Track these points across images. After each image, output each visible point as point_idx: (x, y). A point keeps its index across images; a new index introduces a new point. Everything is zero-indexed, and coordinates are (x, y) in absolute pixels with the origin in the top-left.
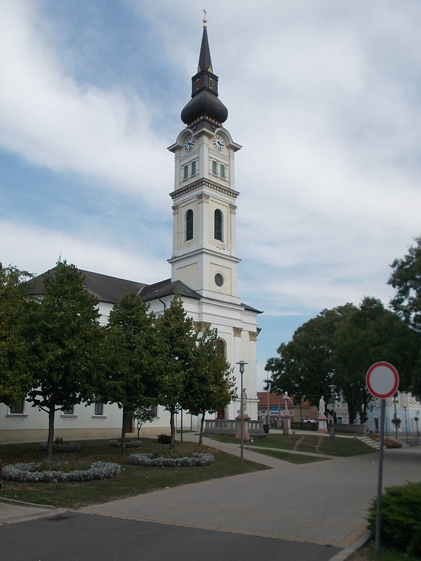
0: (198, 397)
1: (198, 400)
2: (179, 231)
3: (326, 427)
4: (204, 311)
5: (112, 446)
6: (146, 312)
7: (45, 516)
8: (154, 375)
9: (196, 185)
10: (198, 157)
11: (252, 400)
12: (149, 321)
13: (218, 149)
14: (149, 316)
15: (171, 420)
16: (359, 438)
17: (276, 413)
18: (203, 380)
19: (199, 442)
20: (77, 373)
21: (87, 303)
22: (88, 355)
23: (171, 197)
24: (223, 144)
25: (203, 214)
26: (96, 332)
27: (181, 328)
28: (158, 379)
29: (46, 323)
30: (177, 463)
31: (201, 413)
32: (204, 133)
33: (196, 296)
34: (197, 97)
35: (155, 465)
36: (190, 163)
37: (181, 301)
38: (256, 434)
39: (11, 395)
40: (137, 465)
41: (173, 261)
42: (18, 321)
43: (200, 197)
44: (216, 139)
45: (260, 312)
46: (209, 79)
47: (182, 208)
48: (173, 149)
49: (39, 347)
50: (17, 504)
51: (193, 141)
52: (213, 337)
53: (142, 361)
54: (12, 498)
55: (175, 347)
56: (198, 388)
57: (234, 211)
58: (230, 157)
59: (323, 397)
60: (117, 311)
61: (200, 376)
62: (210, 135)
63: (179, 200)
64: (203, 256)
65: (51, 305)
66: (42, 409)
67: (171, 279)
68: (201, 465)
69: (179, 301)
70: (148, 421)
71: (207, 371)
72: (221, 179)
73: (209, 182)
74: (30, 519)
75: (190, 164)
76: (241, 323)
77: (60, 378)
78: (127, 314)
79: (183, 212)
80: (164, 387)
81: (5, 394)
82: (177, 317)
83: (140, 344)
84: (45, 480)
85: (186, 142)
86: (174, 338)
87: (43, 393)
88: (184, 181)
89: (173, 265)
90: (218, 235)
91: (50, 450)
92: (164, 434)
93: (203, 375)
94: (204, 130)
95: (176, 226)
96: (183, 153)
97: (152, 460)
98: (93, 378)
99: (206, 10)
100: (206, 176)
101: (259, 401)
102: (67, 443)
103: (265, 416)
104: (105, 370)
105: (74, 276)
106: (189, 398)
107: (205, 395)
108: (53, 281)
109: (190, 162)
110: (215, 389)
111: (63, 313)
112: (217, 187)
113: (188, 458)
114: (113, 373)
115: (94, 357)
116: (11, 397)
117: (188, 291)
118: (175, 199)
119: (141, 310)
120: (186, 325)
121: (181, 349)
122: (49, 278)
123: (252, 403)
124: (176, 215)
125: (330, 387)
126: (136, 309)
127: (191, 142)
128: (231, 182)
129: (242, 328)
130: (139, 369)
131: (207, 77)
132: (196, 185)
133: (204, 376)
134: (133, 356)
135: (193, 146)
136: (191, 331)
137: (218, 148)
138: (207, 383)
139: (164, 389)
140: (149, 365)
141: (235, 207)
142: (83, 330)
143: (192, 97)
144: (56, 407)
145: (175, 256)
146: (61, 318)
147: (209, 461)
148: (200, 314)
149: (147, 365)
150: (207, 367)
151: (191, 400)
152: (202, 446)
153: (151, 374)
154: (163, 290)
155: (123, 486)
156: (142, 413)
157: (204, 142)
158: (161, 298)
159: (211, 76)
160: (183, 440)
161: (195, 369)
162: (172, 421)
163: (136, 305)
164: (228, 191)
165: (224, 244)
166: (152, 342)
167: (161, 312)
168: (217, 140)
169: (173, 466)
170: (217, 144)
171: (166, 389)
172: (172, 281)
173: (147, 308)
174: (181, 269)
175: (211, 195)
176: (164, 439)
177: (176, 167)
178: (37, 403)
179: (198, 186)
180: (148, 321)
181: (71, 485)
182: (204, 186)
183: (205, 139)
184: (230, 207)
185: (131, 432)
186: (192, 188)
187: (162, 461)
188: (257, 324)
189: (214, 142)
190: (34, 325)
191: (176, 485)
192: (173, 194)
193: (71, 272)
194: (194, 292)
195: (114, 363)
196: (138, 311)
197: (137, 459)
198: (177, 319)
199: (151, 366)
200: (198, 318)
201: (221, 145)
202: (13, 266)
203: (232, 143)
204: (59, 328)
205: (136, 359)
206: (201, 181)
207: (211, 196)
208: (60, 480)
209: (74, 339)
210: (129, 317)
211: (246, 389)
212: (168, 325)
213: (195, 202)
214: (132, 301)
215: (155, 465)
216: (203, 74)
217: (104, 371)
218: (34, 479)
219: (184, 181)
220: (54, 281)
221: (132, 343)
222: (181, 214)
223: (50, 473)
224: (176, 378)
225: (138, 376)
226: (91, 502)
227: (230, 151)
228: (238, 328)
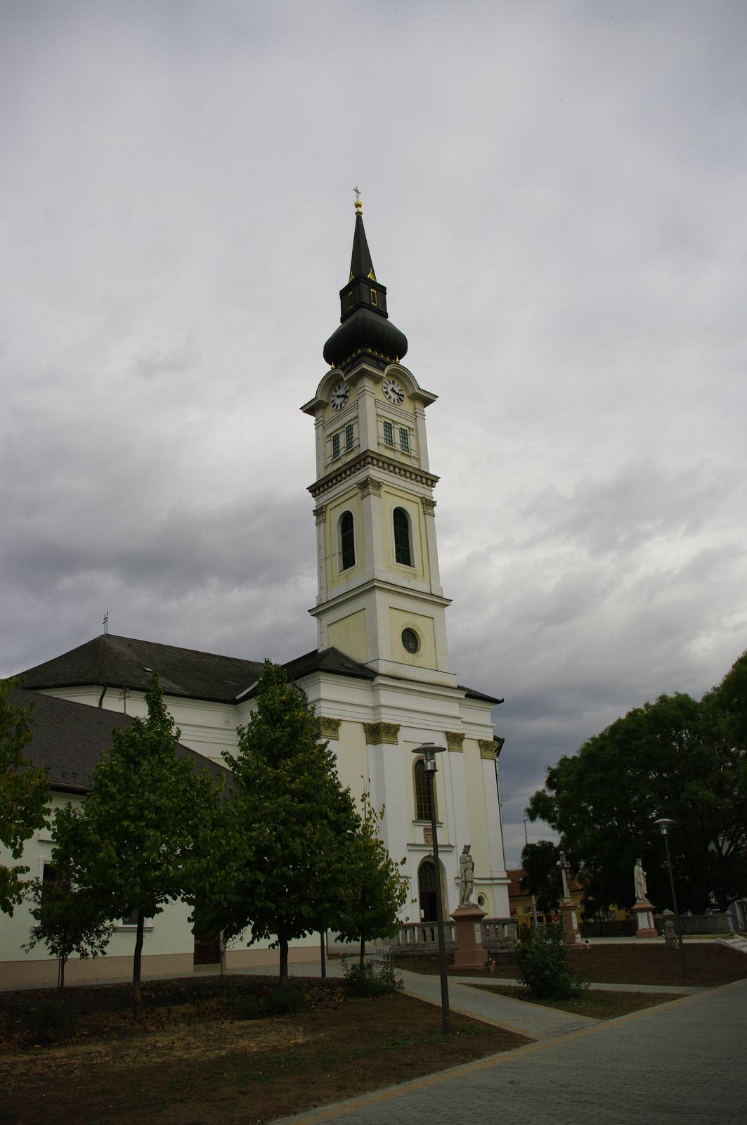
2: (328, 555)
3: (653, 926)
4: (383, 701)
9: (355, 466)
10: (357, 417)
11: (495, 882)
16: (729, 942)
25: (371, 515)
32: (364, 373)
33: (363, 674)
34: (348, 321)
36: (342, 430)
43: (364, 485)
51: (346, 390)
58: (417, 414)
63: (325, 498)
64: (375, 595)
73: (379, 458)
75: (344, 431)
76: (460, 723)
79: (334, 516)
85: (334, 393)
88: (333, 463)
90: (404, 555)
94: (365, 366)
95: (323, 546)
96: (329, 413)
101: (509, 881)
109: (342, 427)
112: (394, 467)
118: (319, 497)
123: (494, 887)
124: (322, 525)
125: (658, 824)
128: (421, 458)
129: (464, 734)
131: (366, 286)
132: (355, 466)
141: (433, 504)
143: (341, 322)
148: (376, 708)
157: (366, 388)
164: (416, 475)
165: (415, 572)
168: (390, 387)
170: (391, 393)
174: (335, 625)
177: (318, 439)
179: (358, 466)
182: (370, 466)
183: (367, 384)
186: (348, 473)
188: (493, 725)
189: (385, 390)
192: (314, 487)
194: (362, 666)
200: (372, 717)
203: (417, 391)
206: (364, 457)
213: (356, 497)
219: (333, 463)
228: (455, 734)
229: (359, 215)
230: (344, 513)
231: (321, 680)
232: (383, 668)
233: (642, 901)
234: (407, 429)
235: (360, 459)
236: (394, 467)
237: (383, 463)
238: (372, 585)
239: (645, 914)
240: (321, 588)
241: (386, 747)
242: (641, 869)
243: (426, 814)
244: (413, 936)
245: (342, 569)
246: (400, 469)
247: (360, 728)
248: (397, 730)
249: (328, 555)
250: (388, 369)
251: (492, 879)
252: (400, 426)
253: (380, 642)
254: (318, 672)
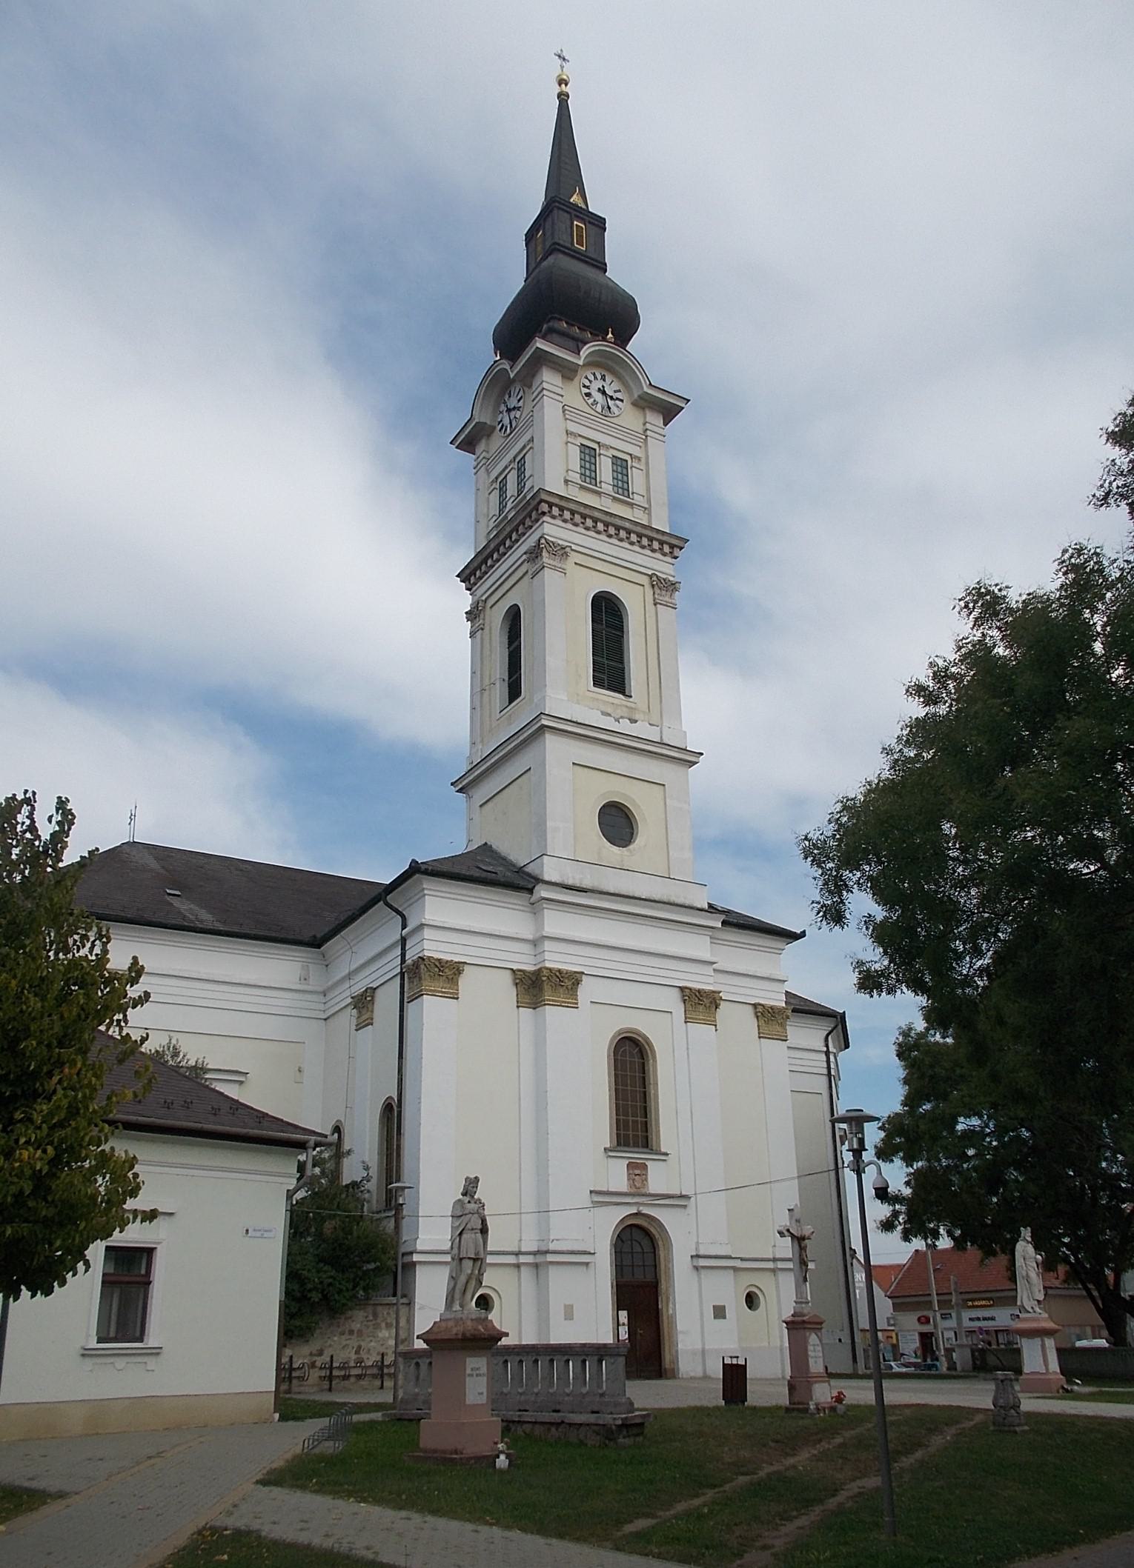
3: (1054, 1366)
4: (549, 929)
10: (532, 440)
13: (599, 409)
17: (985, 1319)
23: (464, 584)
24: (618, 395)
32: (541, 359)
38: (592, 1418)
43: (535, 554)
44: (590, 381)
45: (793, 937)
46: (573, 223)
48: (469, 441)
57: (667, 599)
58: (648, 433)
59: (1026, 1233)
62: (564, 367)
72: (614, 498)
73: (563, 503)
79: (496, 617)
94: (538, 345)
95: (478, 673)
99: (565, 54)
100: (554, 485)
103: (950, 1329)
112: (595, 521)
124: (478, 634)
127: (513, 402)
135: (518, 414)
137: (599, 406)
157: (545, 385)
159: (577, 216)
160: (871, 1384)
165: (633, 705)
170: (598, 397)
175: (574, 547)
179: (528, 522)
182: (546, 518)
183: (549, 379)
184: (653, 586)
194: (520, 871)
200: (531, 960)
201: (611, 398)
203: (646, 389)
207: (572, 550)
211: (477, 1179)
213: (526, 578)
216: (551, 211)
222: (491, 628)
227: (645, 418)
229: (563, 98)
231: (426, 892)
232: (550, 871)
233: (1028, 1315)
234: (628, 458)
235: (529, 509)
236: (595, 521)
237: (573, 512)
238: (539, 725)
239: (1038, 1341)
241: (552, 1014)
242: (1030, 1249)
243: (636, 1136)
246: (607, 525)
247: (508, 977)
248: (577, 983)
249: (487, 682)
250: (585, 351)
251: (775, 1260)
252: (580, 441)
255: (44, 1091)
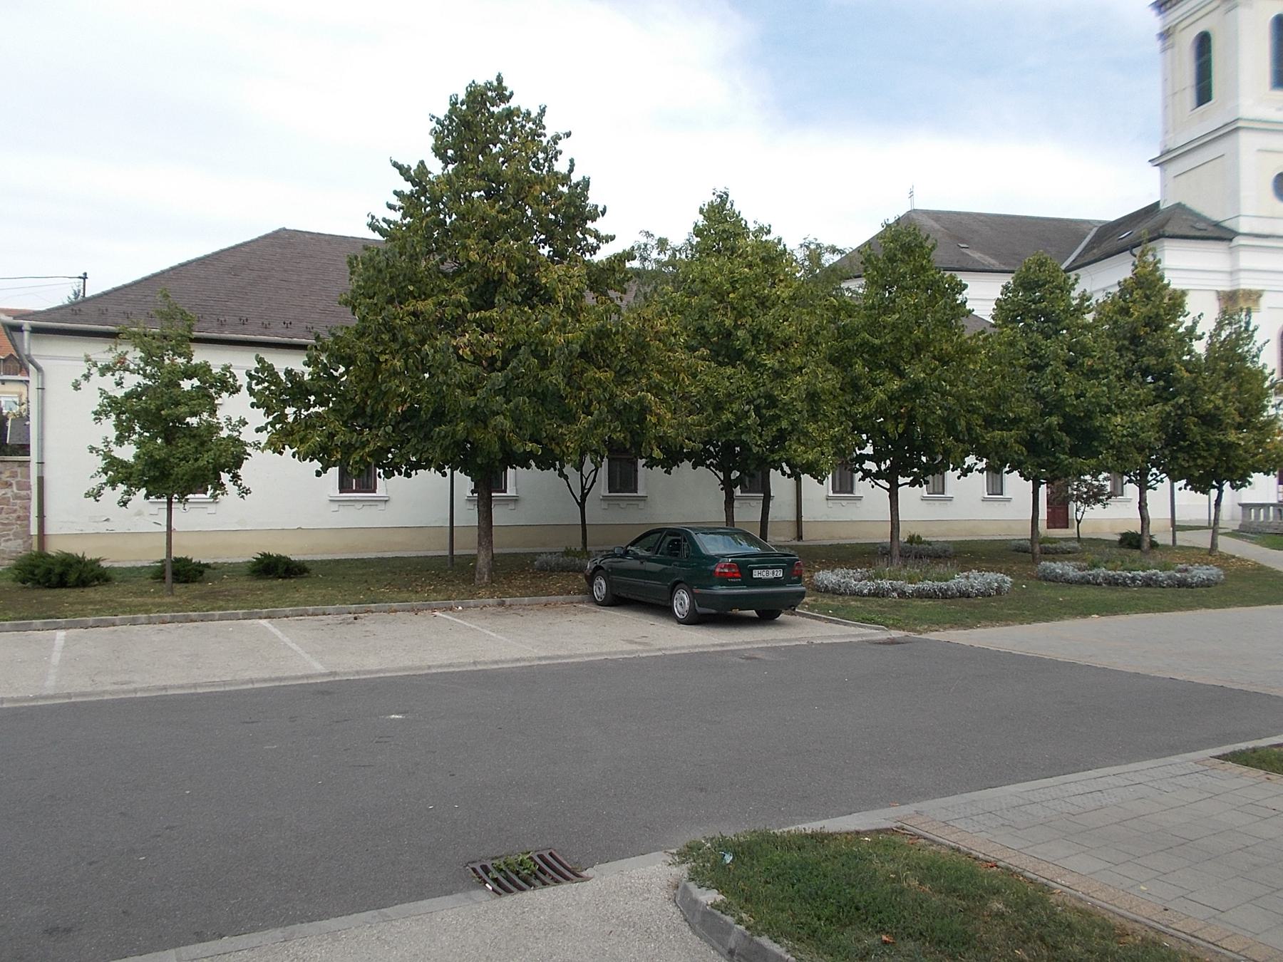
0: (1200, 456)
1: (1199, 462)
5: (1019, 551)
6: (1072, 292)
7: (870, 638)
8: (1089, 415)
12: (1080, 310)
14: (1078, 300)
15: (1139, 503)
18: (1211, 420)
19: (1209, 547)
20: (929, 420)
21: (943, 292)
22: (948, 387)
26: (961, 344)
27: (1157, 315)
28: (1098, 424)
29: (870, 338)
30: (1133, 579)
31: (1214, 487)
33: (1220, 234)
35: (1088, 582)
37: (1158, 258)
39: (817, 461)
40: (1053, 581)
41: (1164, 160)
42: (820, 339)
47: (1183, 32)
49: (861, 379)
50: (831, 621)
52: (1241, 327)
53: (1061, 390)
54: (826, 614)
55: (1143, 356)
56: (1198, 438)
60: (1009, 297)
61: (1203, 413)
65: (876, 303)
66: (876, 484)
67: (1159, 202)
68: (1190, 586)
69: (1151, 259)
70: (1099, 506)
71: (1220, 403)
74: (848, 640)
77: (900, 431)
78: (1029, 301)
79: (1186, 40)
80: (1112, 439)
81: (807, 461)
82: (1146, 294)
83: (1057, 356)
84: (878, 594)
86: (1140, 337)
87: (877, 458)
89: (1163, 171)
91: (896, 552)
92: (1133, 531)
93: (1210, 410)
97: (1081, 573)
98: (959, 428)
102: (929, 543)
104: (981, 412)
105: (916, 245)
106: (1178, 458)
107: (1217, 451)
108: (878, 260)
110: (1243, 439)
111: (897, 316)
113: (1158, 571)
114: (998, 416)
115: (958, 391)
116: (818, 465)
117: (1199, 225)
119: (1058, 291)
120: (1168, 308)
121: (1157, 360)
122: (869, 255)
124: (1169, 52)
126: (1048, 289)
130: (1051, 405)
133: (1213, 411)
134: (1042, 383)
136: (1181, 319)
138: (1221, 425)
139: (1111, 443)
140: (1078, 397)
142: (937, 344)
144: (901, 480)
145: (1168, 147)
146: (894, 326)
147: (1208, 580)
149: (1073, 397)
150: (1220, 394)
151: (1183, 463)
152: (1218, 554)
153: (1082, 414)
154: (1142, 230)
155: (1009, 609)
156: (1086, 490)
158: (1134, 250)
160: (1179, 543)
161: (1189, 399)
162: (1143, 504)
163: (1049, 282)
166: (1085, 352)
167: (1112, 286)
169: (1125, 585)
171: (1117, 442)
172: (1162, 207)
173: (1073, 284)
174: (1183, 176)
176: (1131, 541)
178: (867, 474)
180: (1075, 310)
181: (919, 603)
185: (1068, 527)
187: (1102, 575)
190: (849, 343)
191: (1116, 613)
193: (909, 238)
194: (1217, 225)
195: (999, 399)
196: (1053, 293)
197: (1054, 569)
198: (1148, 297)
199: (1082, 399)
202: (811, 239)
204: (892, 343)
205: (1049, 387)
208: (902, 594)
209: (920, 360)
210: (1033, 307)
212: (1125, 311)
213: (1217, 12)
214: (1040, 275)
215: (1088, 582)
217: (978, 414)
218: (862, 592)
220: (879, 259)
221: (1040, 358)
223: (886, 584)
224: (1138, 419)
225: (1054, 420)
226: (947, 626)
230: (1201, 33)
240: (1166, 80)
244: (1267, 516)
245: (1194, 104)
247: (1213, 297)
253: (1243, 194)
254: (1161, 239)
255: (861, 356)
